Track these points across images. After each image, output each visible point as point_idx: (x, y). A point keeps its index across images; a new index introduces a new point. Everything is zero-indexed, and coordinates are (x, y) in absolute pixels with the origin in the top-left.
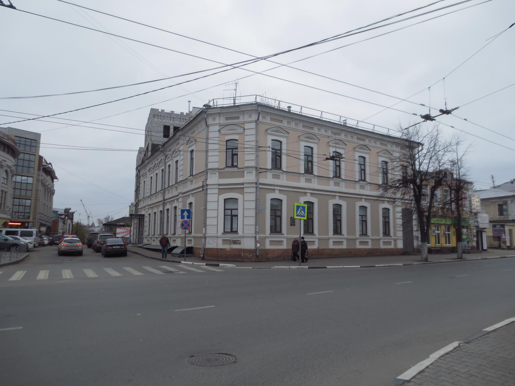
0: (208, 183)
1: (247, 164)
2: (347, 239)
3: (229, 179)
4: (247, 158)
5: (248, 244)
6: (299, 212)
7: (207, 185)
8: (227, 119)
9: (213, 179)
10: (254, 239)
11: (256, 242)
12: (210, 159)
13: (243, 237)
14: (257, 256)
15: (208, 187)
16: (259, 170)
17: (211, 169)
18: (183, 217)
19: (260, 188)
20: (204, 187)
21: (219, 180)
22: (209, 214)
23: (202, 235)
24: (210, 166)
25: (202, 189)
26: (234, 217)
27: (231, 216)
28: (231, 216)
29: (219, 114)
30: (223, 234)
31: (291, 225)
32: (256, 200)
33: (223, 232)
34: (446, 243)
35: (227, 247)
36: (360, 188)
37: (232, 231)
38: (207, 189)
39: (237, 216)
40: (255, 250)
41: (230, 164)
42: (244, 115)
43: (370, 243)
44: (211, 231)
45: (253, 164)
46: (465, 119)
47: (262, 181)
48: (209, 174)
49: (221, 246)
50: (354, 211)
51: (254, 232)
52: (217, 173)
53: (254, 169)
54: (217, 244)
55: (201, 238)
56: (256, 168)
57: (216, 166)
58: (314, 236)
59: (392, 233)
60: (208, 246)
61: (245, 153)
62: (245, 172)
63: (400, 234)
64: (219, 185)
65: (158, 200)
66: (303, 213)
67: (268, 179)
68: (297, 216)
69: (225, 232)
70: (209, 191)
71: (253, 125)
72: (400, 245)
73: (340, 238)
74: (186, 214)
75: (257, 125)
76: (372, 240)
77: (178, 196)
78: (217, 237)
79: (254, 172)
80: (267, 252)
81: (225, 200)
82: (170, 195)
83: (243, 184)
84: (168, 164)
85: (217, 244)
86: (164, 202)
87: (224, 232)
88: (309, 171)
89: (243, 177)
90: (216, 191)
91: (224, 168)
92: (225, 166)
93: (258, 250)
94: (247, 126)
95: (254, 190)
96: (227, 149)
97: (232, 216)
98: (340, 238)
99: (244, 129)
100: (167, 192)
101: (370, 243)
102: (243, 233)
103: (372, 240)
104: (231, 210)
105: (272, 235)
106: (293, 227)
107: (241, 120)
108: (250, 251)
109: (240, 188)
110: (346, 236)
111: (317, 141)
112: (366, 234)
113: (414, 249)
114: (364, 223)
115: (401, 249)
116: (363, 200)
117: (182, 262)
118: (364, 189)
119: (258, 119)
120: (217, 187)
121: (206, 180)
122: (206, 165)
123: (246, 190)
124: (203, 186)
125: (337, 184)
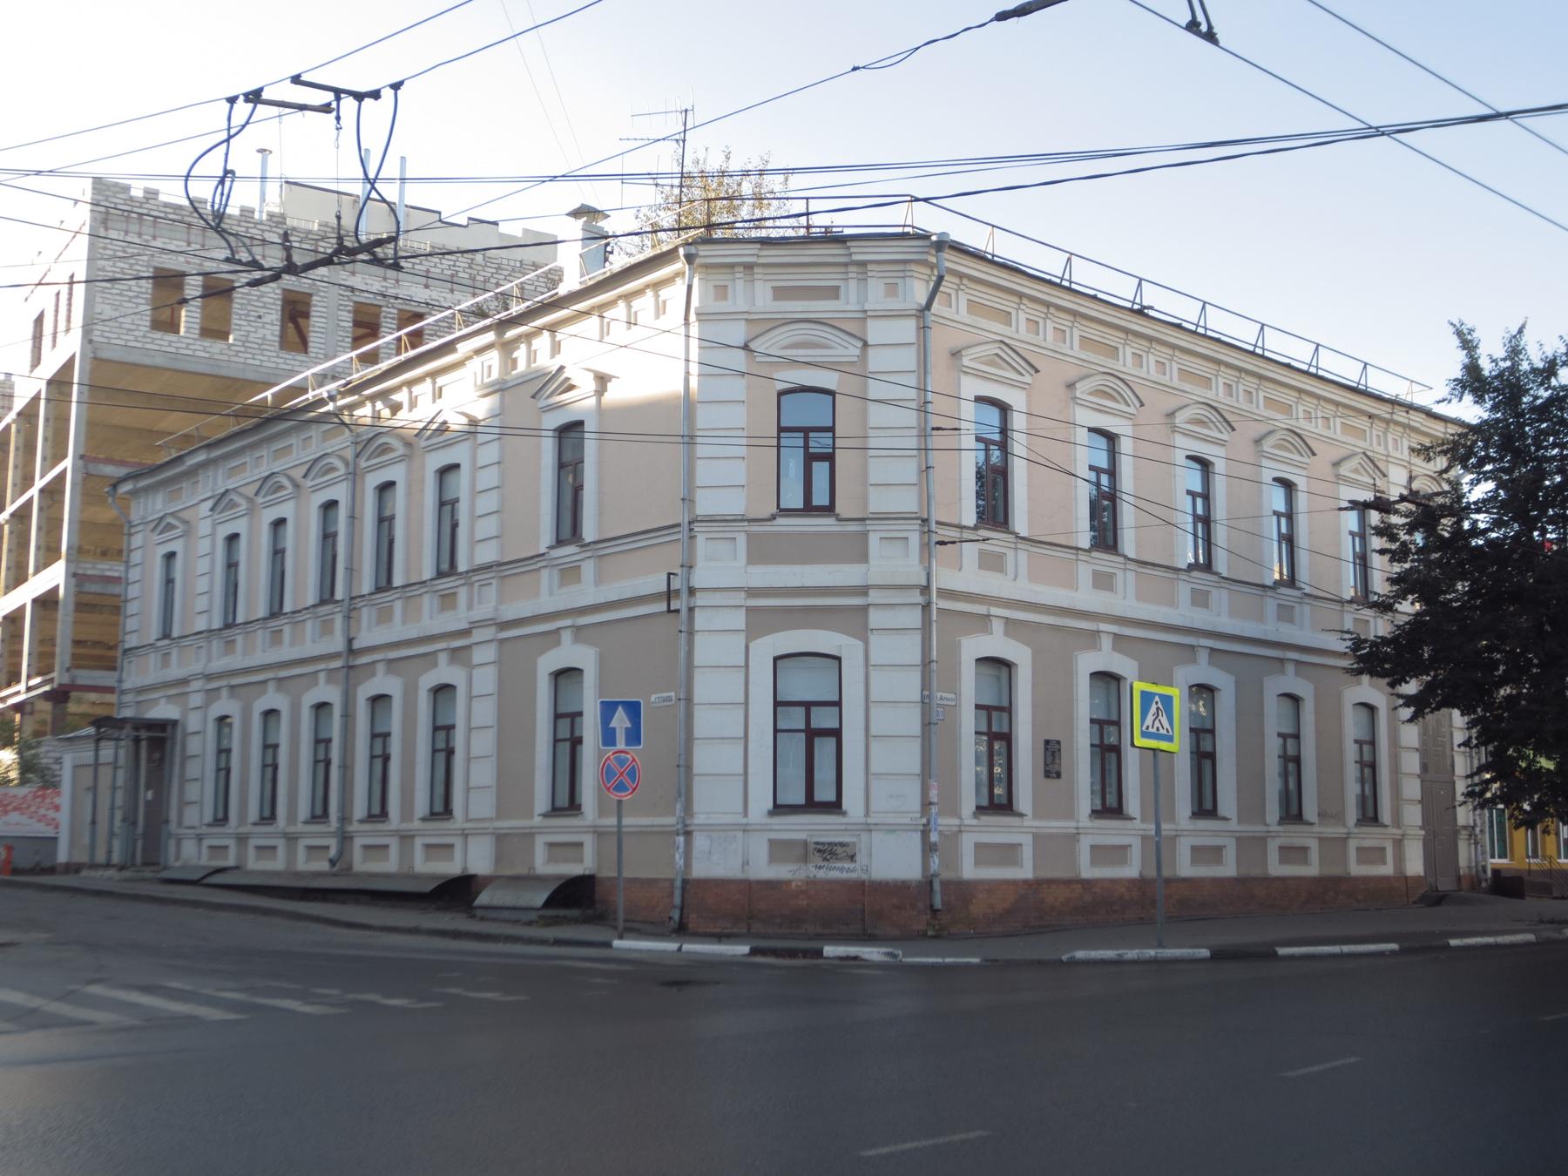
0: (697, 582)
1: (879, 502)
2: (599, 833)
3: (797, 568)
4: (881, 479)
5: (893, 860)
6: (1149, 721)
7: (692, 591)
8: (780, 293)
9: (721, 566)
10: (917, 837)
11: (928, 848)
12: (705, 473)
13: (868, 828)
14: (934, 911)
15: (700, 600)
16: (933, 536)
17: (711, 520)
18: (608, 737)
19: (937, 614)
20: (676, 601)
21: (754, 569)
22: (704, 722)
23: (671, 820)
24: (706, 505)
25: (663, 607)
26: (817, 740)
27: (811, 730)
28: (811, 730)
29: (749, 267)
30: (772, 813)
31: (1048, 774)
32: (926, 663)
33: (771, 806)
34: (1493, 856)
35: (781, 872)
36: (1280, 618)
37: (811, 805)
38: (691, 610)
39: (837, 733)
40: (928, 883)
41: (794, 498)
42: (863, 280)
43: (1314, 855)
44: (713, 802)
45: (908, 502)
46: (855, 69)
47: (945, 578)
48: (700, 540)
49: (763, 869)
50: (1070, 701)
51: (915, 804)
52: (742, 540)
53: (916, 525)
54: (746, 863)
55: (667, 834)
56: (925, 521)
57: (734, 504)
58: (1128, 824)
59: (1386, 815)
60: (700, 871)
61: (872, 452)
62: (874, 539)
63: (1413, 815)
64: (752, 592)
65: (310, 648)
66: (1166, 724)
67: (963, 572)
68: (1145, 735)
69: (779, 809)
70: (701, 620)
71: (906, 330)
72: (1415, 865)
73: (1216, 833)
74: (620, 721)
75: (923, 328)
76: (1321, 840)
77: (465, 633)
78: (746, 829)
79: (915, 539)
80: (962, 891)
81: (776, 659)
82: (397, 630)
83: (863, 590)
84: (373, 480)
85: (746, 863)
86: (352, 663)
87: (776, 805)
88: (1106, 536)
89: (863, 557)
90: (739, 620)
91: (774, 517)
92: (774, 510)
93: (937, 887)
94: (876, 331)
95: (914, 618)
96: (781, 429)
97: (812, 734)
98: (1216, 833)
99: (866, 344)
100: (366, 614)
101: (1314, 855)
102: (867, 814)
103: (1321, 840)
104: (808, 705)
105: (1364, 829)
106: (1053, 783)
107: (850, 299)
108: (898, 889)
109: (851, 613)
110: (1233, 825)
111: (1132, 410)
112: (574, 807)
113: (1459, 879)
114: (1207, 764)
115: (1418, 879)
116: (1290, 668)
117: (617, 943)
118: (1291, 620)
119: (928, 306)
120: (739, 598)
121: (689, 567)
122: (688, 500)
123: (876, 618)
124: (669, 594)
125: (1103, 581)
